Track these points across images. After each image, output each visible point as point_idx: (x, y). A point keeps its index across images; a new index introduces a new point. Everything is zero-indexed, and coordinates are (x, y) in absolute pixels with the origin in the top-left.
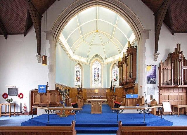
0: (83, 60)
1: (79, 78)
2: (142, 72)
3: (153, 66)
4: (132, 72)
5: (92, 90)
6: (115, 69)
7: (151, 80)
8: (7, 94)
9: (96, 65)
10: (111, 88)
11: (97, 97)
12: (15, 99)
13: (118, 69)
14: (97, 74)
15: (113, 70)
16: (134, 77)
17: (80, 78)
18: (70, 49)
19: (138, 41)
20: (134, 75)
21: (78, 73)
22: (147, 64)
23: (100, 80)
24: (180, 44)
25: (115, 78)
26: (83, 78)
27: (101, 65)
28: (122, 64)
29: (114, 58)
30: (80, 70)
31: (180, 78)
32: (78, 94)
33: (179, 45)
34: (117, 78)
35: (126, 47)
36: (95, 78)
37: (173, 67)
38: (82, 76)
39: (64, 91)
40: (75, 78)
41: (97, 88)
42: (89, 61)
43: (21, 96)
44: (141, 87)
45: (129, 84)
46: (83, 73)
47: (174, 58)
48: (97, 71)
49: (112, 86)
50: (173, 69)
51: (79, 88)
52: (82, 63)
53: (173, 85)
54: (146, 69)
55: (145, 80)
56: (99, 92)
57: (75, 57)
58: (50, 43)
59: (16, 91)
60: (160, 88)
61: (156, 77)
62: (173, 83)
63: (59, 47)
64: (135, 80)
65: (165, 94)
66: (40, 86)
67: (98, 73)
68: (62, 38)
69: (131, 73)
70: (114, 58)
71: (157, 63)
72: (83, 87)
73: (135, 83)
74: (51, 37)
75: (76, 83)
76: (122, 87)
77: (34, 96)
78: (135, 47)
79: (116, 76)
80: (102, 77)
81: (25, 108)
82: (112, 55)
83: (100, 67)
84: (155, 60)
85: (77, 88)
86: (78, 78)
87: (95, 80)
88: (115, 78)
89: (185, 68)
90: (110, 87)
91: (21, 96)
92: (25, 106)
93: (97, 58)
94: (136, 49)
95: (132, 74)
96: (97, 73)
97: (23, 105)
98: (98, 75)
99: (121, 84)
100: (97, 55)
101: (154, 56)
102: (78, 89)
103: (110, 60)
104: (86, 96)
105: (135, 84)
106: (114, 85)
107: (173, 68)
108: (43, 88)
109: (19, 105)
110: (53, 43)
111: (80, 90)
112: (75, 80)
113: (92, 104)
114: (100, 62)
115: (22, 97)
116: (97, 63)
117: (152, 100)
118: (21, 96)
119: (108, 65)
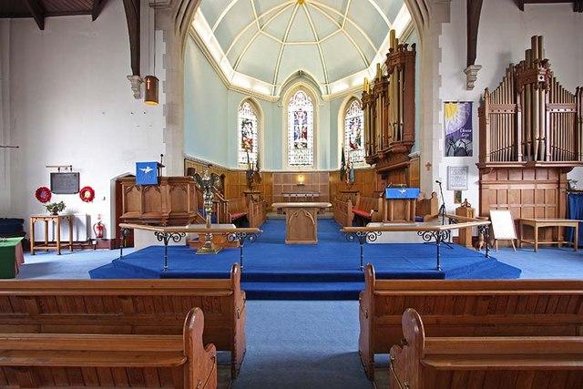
0: (263, 89)
1: (251, 142)
3: (464, 105)
6: (354, 115)
7: (456, 145)
9: (299, 103)
10: (343, 171)
12: (72, 203)
15: (348, 116)
16: (407, 138)
20: (408, 130)
22: (446, 99)
23: (310, 146)
25: (353, 141)
27: (314, 102)
28: (373, 99)
29: (350, 82)
30: (253, 118)
32: (251, 187)
33: (537, 41)
34: (358, 140)
35: (386, 47)
36: (297, 141)
37: (519, 106)
39: (208, 179)
40: (240, 142)
42: (279, 92)
43: (88, 194)
44: (429, 165)
45: (393, 159)
47: (524, 78)
48: (301, 121)
49: (344, 164)
50: (519, 114)
51: (252, 171)
52: (262, 98)
53: (520, 159)
54: (441, 113)
56: (307, 181)
57: (240, 81)
59: (74, 181)
60: (483, 169)
61: (470, 138)
62: (520, 154)
63: (189, 41)
64: (410, 146)
65: (498, 187)
66: (139, 165)
67: (305, 126)
68: (199, 23)
70: (350, 82)
71: (474, 95)
72: (263, 169)
74: (168, 21)
75: (242, 155)
78: (410, 49)
79: (355, 135)
81: (101, 228)
82: (345, 72)
83: (309, 108)
84: (470, 88)
87: (296, 146)
88: (353, 141)
90: (339, 168)
91: (88, 194)
92: (99, 224)
93: (300, 83)
94: (414, 53)
95: (401, 127)
96: (301, 126)
97: (94, 221)
98: (306, 133)
99: (371, 159)
100: (300, 75)
102: (250, 172)
103: (339, 87)
105: (411, 158)
108: (148, 170)
110: (176, 37)
111: (253, 176)
114: (310, 94)
115: (91, 199)
117: (459, 205)
118: (88, 195)
119: (335, 102)
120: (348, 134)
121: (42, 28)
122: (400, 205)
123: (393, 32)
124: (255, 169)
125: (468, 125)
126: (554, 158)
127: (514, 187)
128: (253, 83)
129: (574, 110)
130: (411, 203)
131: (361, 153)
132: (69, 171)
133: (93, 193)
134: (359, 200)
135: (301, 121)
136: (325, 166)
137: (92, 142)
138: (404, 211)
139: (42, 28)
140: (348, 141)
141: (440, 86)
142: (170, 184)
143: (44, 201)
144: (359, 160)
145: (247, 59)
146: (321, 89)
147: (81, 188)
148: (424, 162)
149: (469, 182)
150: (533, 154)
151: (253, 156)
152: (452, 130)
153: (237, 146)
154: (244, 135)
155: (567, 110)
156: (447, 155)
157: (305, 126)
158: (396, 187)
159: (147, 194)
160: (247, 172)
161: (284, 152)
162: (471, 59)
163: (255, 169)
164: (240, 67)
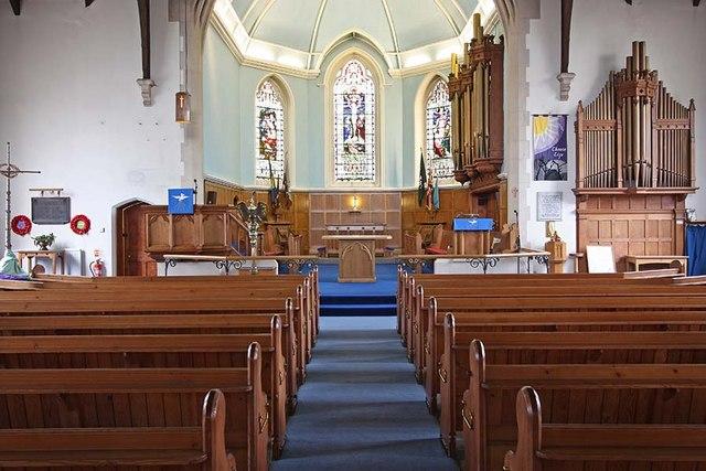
0: (292, 60)
2: (517, 141)
3: (556, 119)
4: (487, 134)
5: (334, 199)
7: (548, 166)
8: (30, 218)
9: (352, 80)
10: (422, 191)
11: (626, 323)
12: (63, 234)
13: (443, 100)
14: (354, 122)
16: (494, 154)
17: (279, 143)
18: (240, 24)
19: (504, 22)
20: (495, 144)
21: (268, 122)
22: (537, 108)
23: (369, 149)
24: (641, 44)
25: (439, 143)
26: (293, 142)
27: (376, 79)
28: (459, 86)
29: (433, 53)
30: (277, 106)
31: (640, 162)
32: (274, 215)
33: (639, 47)
34: (446, 143)
35: (468, 34)
36: (349, 141)
37: (619, 122)
38: (286, 131)
39: (254, 208)
40: (258, 146)
41: (357, 189)
43: (81, 225)
44: (516, 191)
45: (483, 183)
46: (292, 118)
47: (626, 87)
48: (354, 110)
49: (423, 180)
50: (619, 131)
51: (276, 190)
52: (292, 74)
53: (620, 184)
54: (529, 129)
55: (528, 166)
56: (365, 205)
57: (257, 51)
58: (185, 32)
59: (62, 208)
60: (580, 198)
61: (564, 159)
62: (620, 179)
63: (209, 32)
64: (498, 166)
66: (172, 193)
67: (362, 117)
69: (484, 141)
70: (433, 53)
71: (568, 107)
72: (293, 187)
73: (500, 176)
75: (261, 164)
76: (466, 184)
77: (150, 225)
78: (496, 41)
79: (442, 135)
80: (377, 135)
81: (100, 266)
83: (367, 89)
84: (564, 98)
85: (268, 187)
86: (271, 145)
87: (347, 149)
89: (665, 127)
90: (417, 185)
91: (81, 225)
92: (98, 261)
93: (354, 48)
94: (502, 45)
96: (354, 118)
97: (91, 259)
98: (363, 129)
99: (461, 175)
100: (354, 37)
101: (561, 80)
102: (273, 192)
103: (416, 59)
104: (307, 227)
105: (500, 180)
106: (433, 174)
107: (619, 126)
108: (182, 197)
109: (78, 257)
110: (195, 31)
111: (278, 199)
112: (258, 151)
113: (343, 251)
114: (369, 66)
115: (86, 230)
116: (353, 68)
117: (549, 239)
118: (82, 225)
119: (410, 80)
120: (430, 132)
121: (17, 12)
122: (473, 238)
123: (478, 17)
124: (281, 186)
125: (562, 142)
126: (662, 181)
127: (651, 217)
128: (277, 54)
129: (687, 127)
130: (485, 237)
131: (449, 163)
132: (56, 195)
133: (88, 223)
134: (440, 234)
135: (354, 110)
136: (394, 182)
137: (98, 161)
138: (478, 243)
139: (17, 12)
140: (431, 142)
141: (528, 95)
142: (202, 212)
143: (23, 232)
144: (445, 175)
145: (267, 18)
146: (386, 56)
147: (72, 217)
148: (510, 189)
149: (564, 209)
150: (634, 178)
151: (278, 166)
152: (543, 148)
153: (253, 152)
154: (263, 133)
155: (679, 127)
156: (537, 179)
157: (362, 117)
158: (465, 217)
159: (178, 225)
160: (270, 191)
161: (327, 158)
162: (564, 69)
163: (281, 186)
164: (257, 32)
